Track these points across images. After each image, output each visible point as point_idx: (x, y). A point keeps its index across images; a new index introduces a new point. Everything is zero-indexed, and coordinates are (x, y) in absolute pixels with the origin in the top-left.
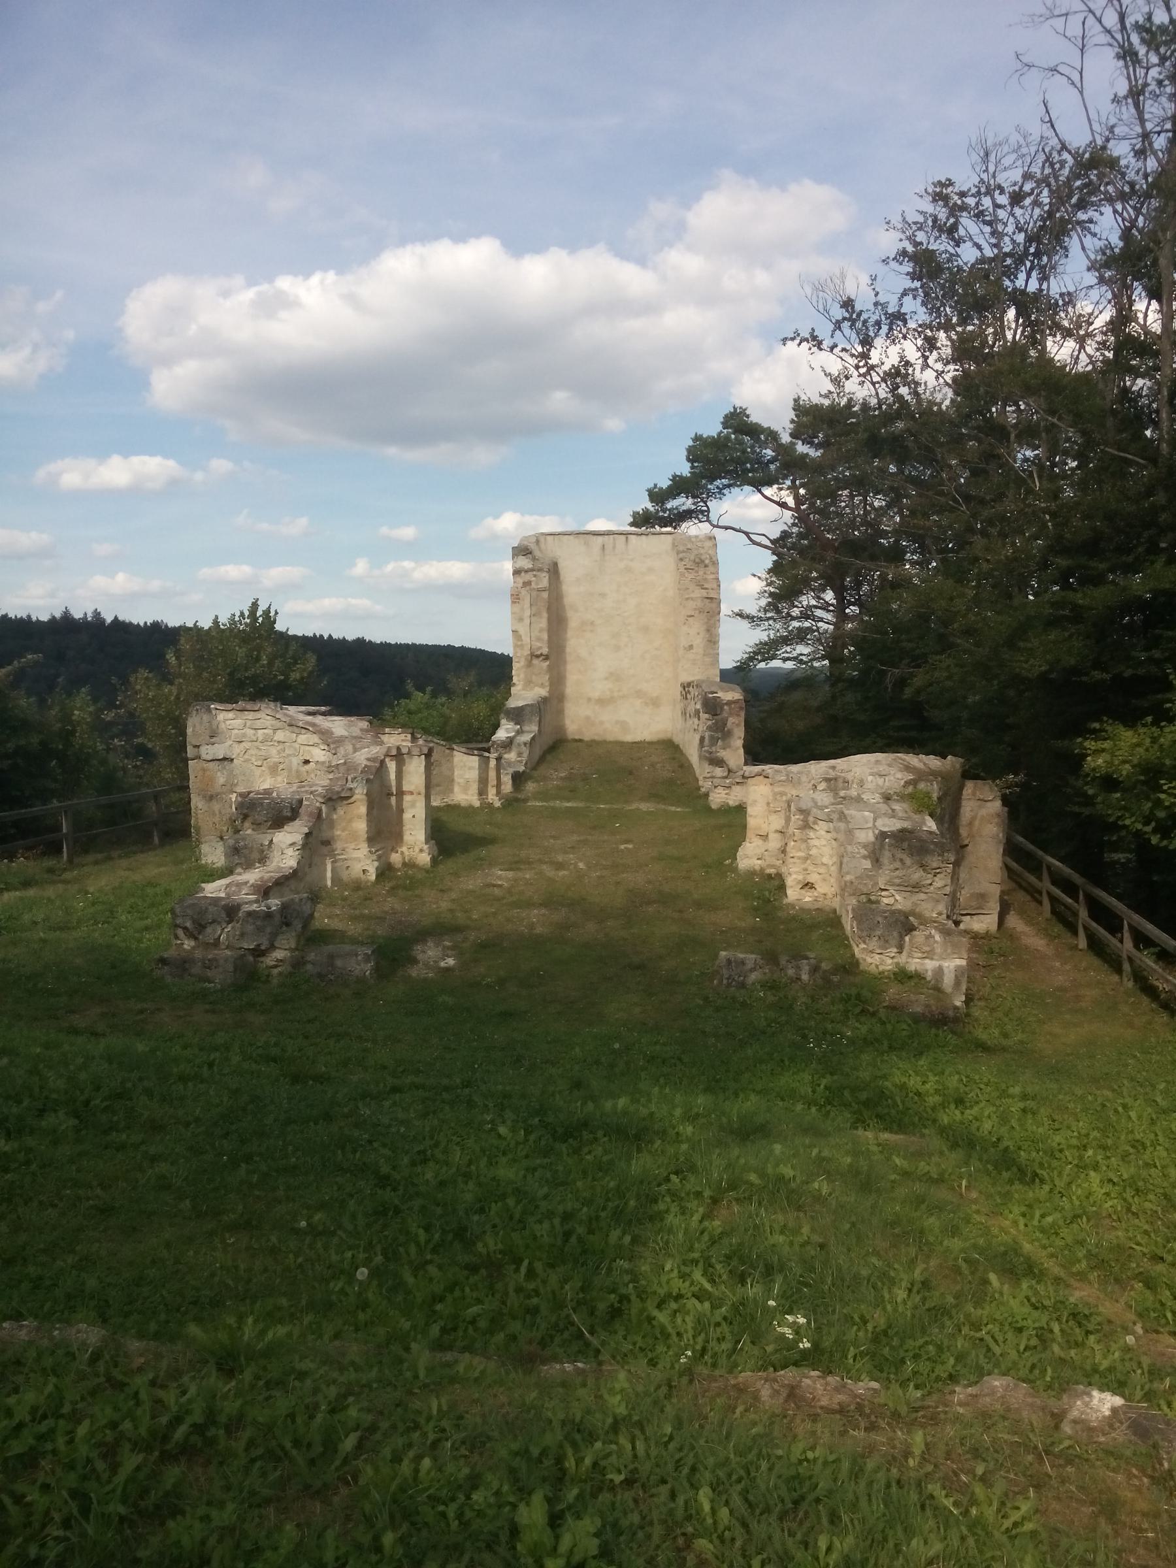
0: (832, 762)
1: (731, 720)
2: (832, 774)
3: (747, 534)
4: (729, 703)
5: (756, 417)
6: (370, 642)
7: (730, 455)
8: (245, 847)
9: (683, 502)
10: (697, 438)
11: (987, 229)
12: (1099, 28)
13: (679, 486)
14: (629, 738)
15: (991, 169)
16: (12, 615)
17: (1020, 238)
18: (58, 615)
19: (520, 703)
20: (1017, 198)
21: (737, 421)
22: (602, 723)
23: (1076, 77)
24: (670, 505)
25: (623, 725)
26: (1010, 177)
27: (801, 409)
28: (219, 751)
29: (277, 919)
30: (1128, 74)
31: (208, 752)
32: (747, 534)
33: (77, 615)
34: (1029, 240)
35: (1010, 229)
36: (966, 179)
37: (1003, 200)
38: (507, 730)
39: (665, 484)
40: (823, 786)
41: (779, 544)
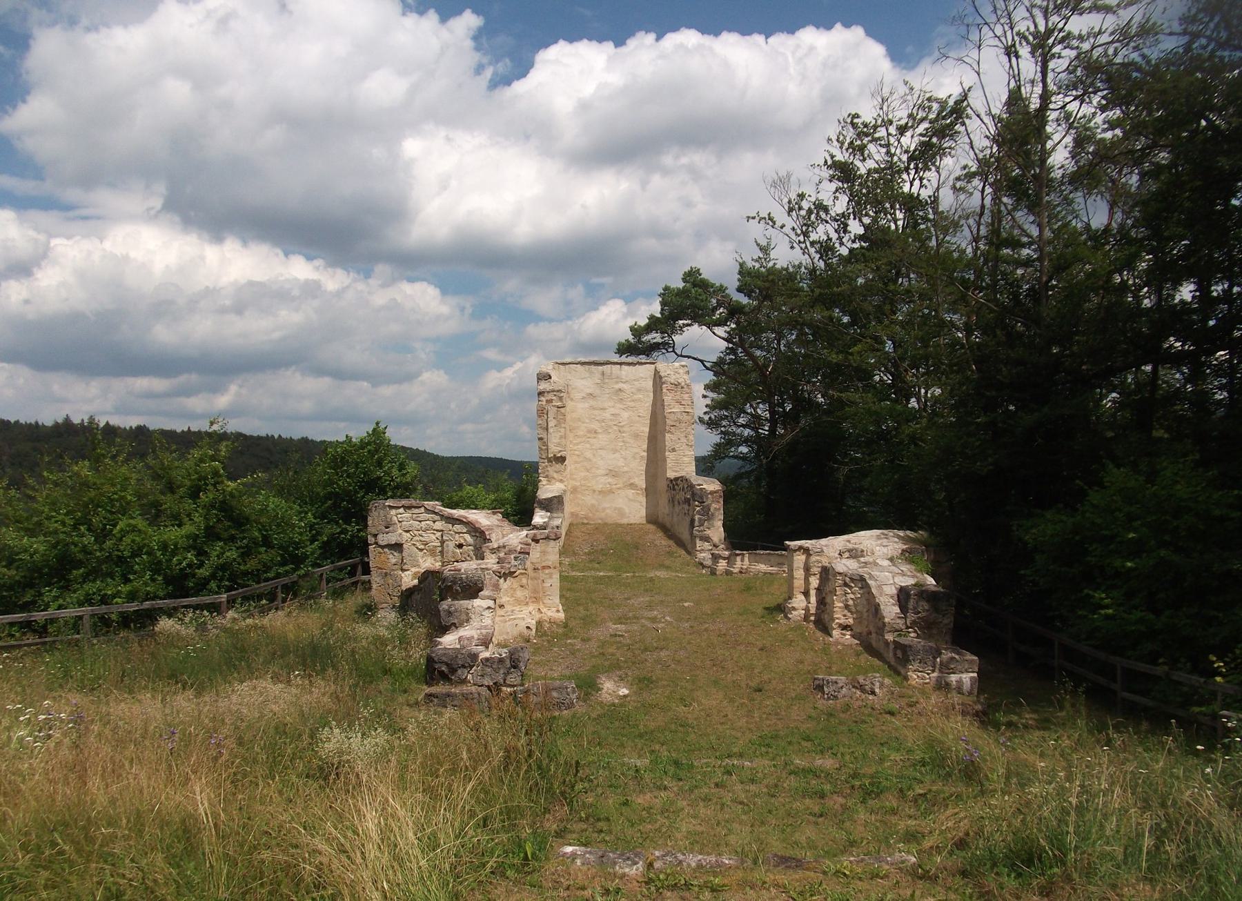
0: (845, 537)
1: (714, 506)
2: (850, 546)
3: (702, 361)
4: (712, 493)
5: (705, 275)
6: (17, 422)
7: (689, 301)
8: (456, 611)
9: (655, 337)
10: (666, 288)
11: (884, 150)
12: (991, 34)
13: (654, 324)
14: (625, 521)
15: (885, 108)
16: (22, 421)
17: (905, 158)
18: (60, 421)
19: (549, 495)
20: (902, 130)
21: (692, 277)
22: (604, 509)
23: (976, 68)
24: (645, 338)
25: (621, 512)
26: (901, 115)
27: (744, 271)
28: (392, 538)
29: (508, 663)
30: (1011, 66)
31: (384, 539)
32: (702, 361)
33: (76, 420)
34: (910, 159)
35: (898, 152)
36: (868, 115)
37: (892, 130)
38: (542, 517)
39: (643, 322)
40: (847, 555)
41: (718, 367)
